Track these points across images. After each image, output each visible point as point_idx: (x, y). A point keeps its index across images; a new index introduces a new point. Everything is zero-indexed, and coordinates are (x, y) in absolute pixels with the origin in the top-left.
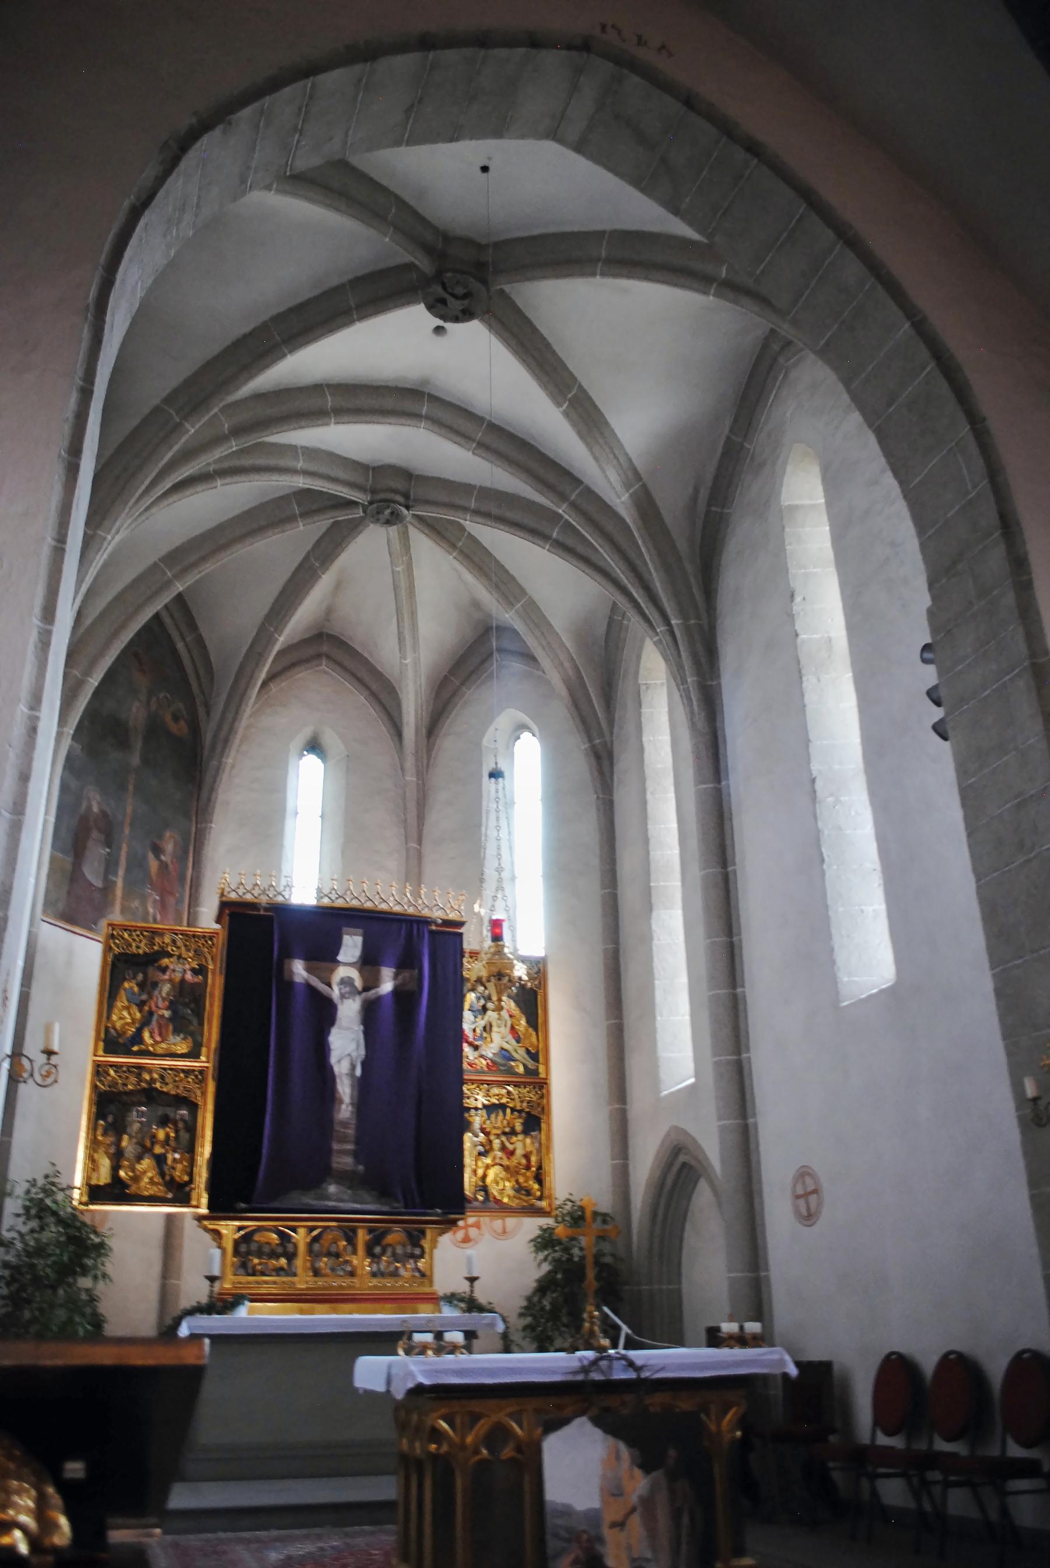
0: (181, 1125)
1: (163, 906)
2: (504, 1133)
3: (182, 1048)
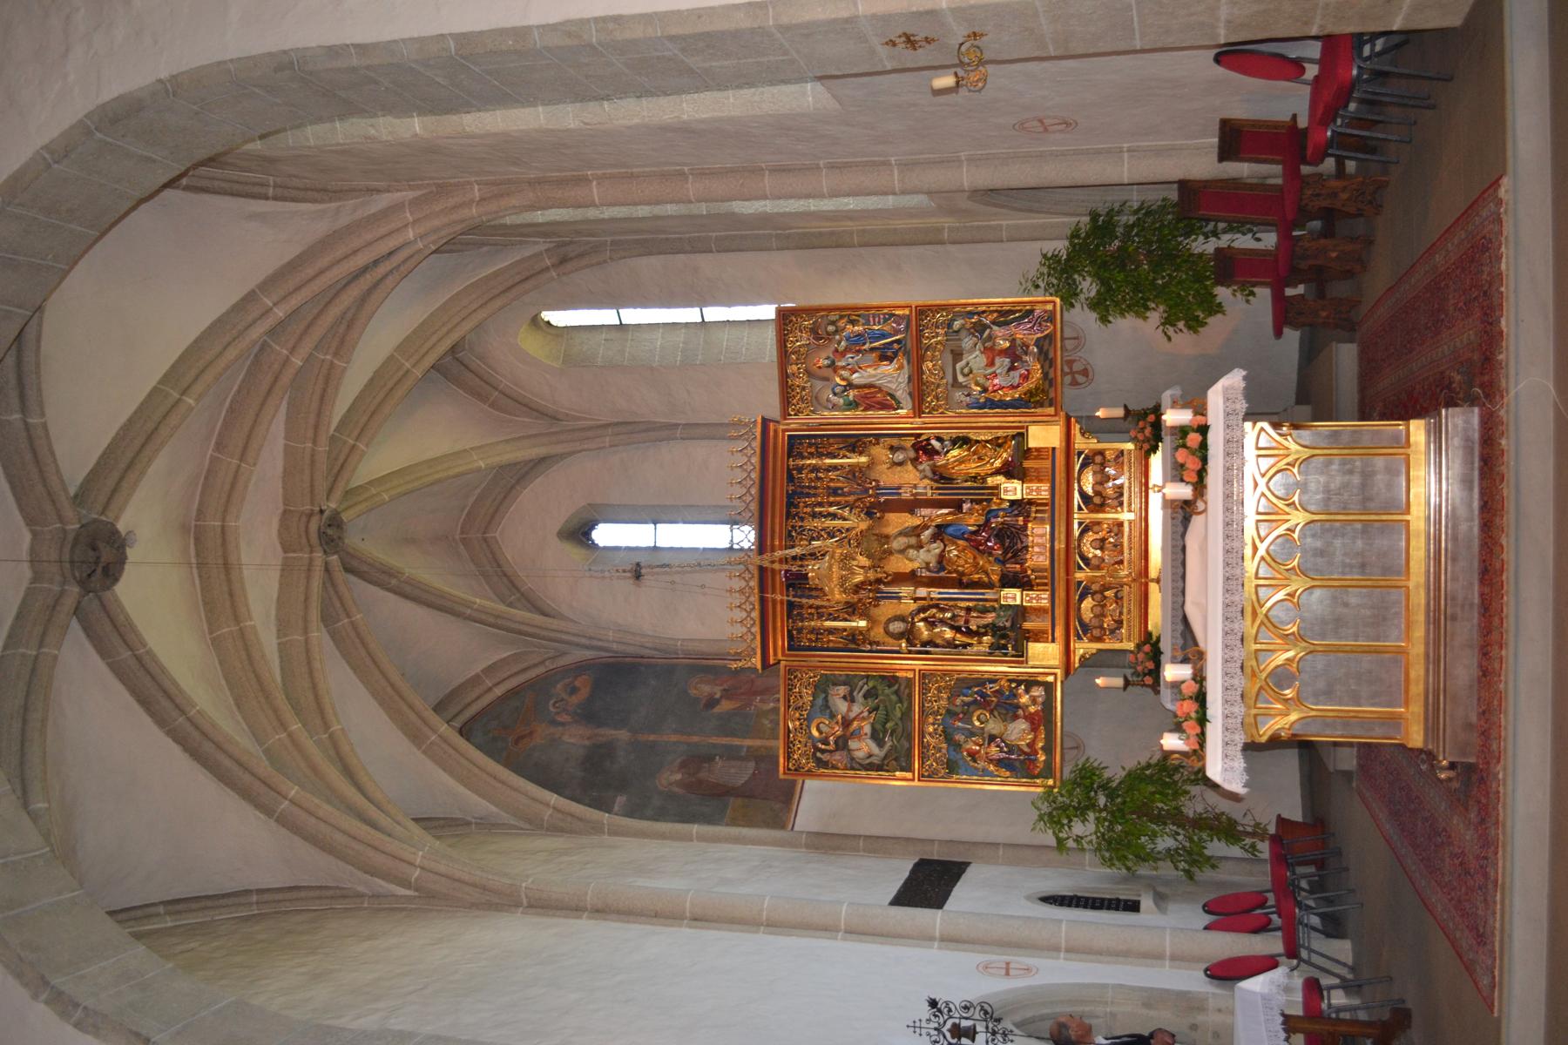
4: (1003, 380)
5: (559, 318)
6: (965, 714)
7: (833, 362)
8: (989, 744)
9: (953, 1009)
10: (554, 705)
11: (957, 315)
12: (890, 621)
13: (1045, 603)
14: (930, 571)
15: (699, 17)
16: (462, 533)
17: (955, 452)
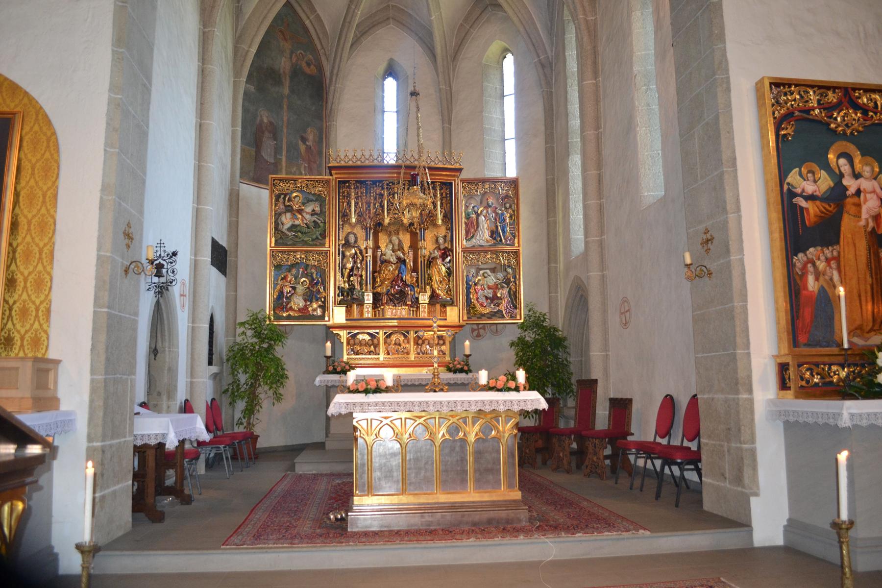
4: (481, 294)
5: (509, 62)
6: (306, 274)
7: (490, 206)
8: (291, 287)
9: (172, 265)
10: (301, 53)
11: (514, 270)
12: (355, 235)
13: (366, 315)
14: (381, 256)
15: (728, 132)
16: (393, 6)
17: (444, 269)
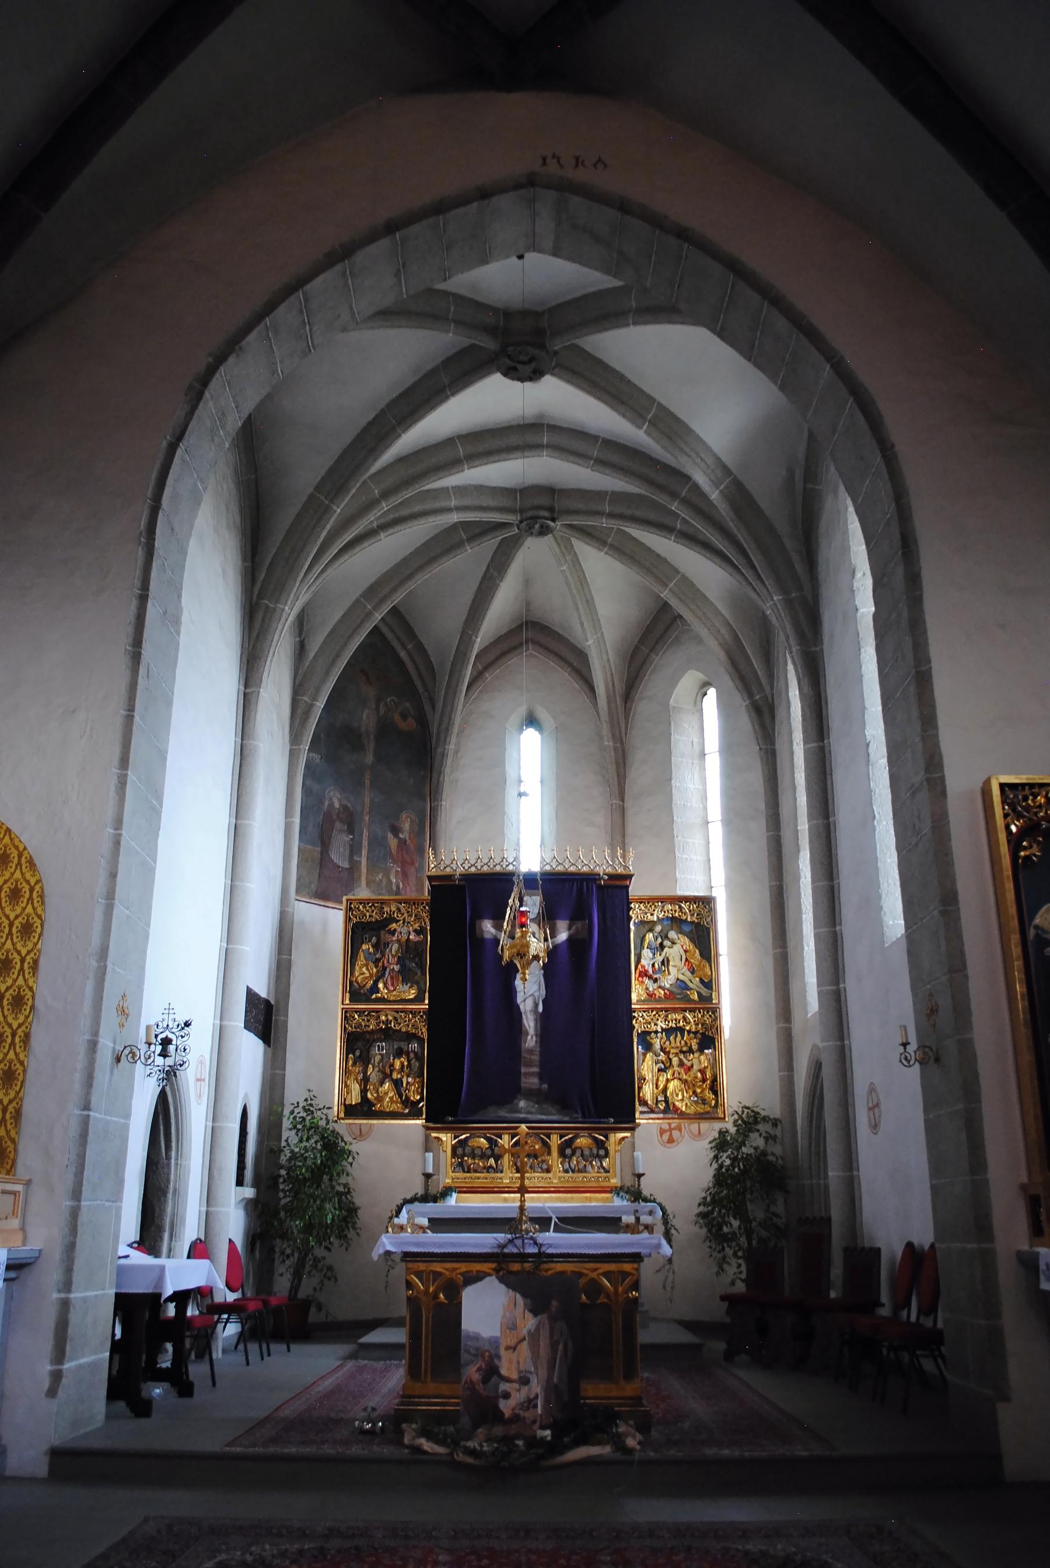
0: (412, 1055)
1: (405, 875)
2: (682, 1052)
3: (412, 994)
9: (184, 1039)
10: (393, 701)
